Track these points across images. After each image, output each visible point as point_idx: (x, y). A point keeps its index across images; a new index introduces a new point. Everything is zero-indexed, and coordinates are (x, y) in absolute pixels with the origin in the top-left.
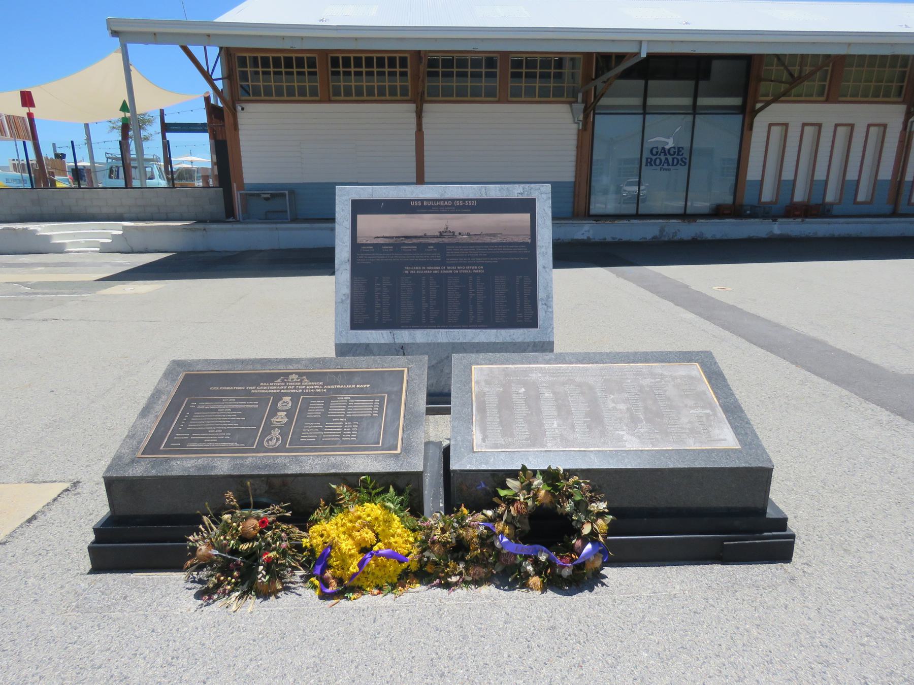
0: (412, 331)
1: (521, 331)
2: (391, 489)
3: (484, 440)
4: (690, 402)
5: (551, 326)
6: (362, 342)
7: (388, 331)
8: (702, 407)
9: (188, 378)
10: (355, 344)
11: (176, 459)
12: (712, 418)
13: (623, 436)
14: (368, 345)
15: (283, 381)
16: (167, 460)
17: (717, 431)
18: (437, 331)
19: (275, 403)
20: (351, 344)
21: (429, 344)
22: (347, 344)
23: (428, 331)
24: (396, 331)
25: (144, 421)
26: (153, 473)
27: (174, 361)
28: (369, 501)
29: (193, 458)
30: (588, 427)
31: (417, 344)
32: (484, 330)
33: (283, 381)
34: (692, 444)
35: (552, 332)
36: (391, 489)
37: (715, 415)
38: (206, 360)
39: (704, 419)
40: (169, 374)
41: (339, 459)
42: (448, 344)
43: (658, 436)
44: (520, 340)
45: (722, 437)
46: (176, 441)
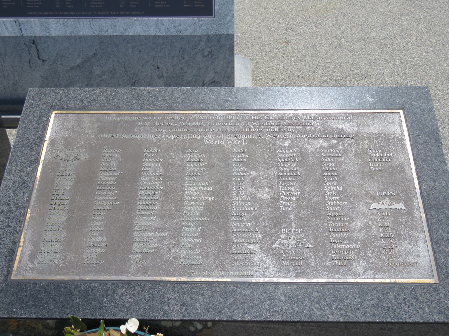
0: (43, 19)
1: (189, 20)
3: (32, 258)
4: (374, 188)
5: (230, 13)
7: (12, 20)
8: (391, 198)
12: (403, 219)
13: (253, 254)
17: (405, 247)
18: (77, 19)
21: (69, 38)
23: (66, 19)
24: (22, 20)
30: (202, 234)
31: (54, 38)
32: (140, 19)
34: (362, 276)
35: (231, 21)
37: (409, 212)
39: (390, 223)
43: (309, 255)
44: (188, 33)
45: (410, 259)
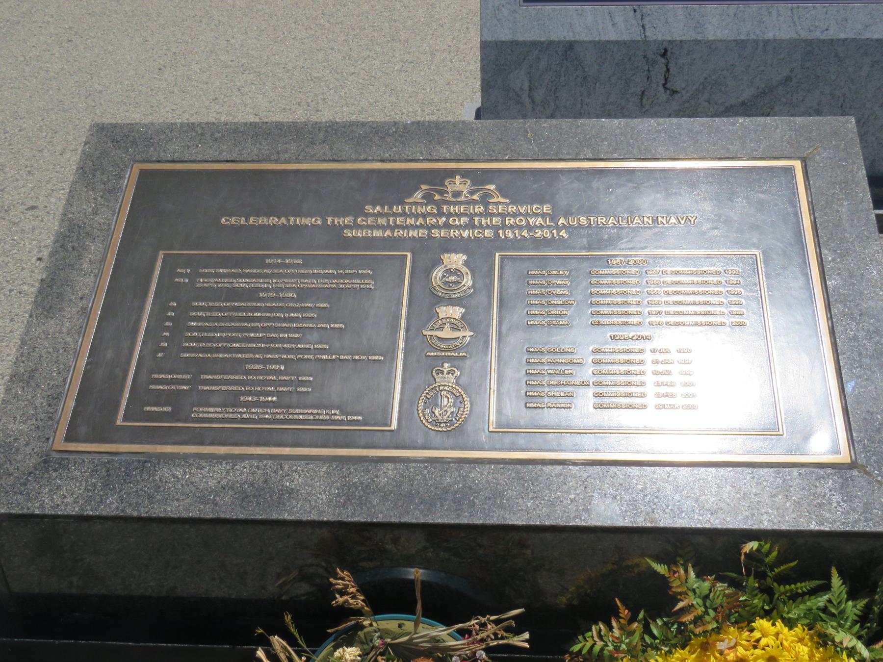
2: (836, 581)
6: (554, 37)
9: (151, 185)
10: (535, 44)
11: (170, 458)
14: (570, 46)
15: (428, 198)
16: (148, 462)
19: (422, 272)
20: (524, 43)
22: (515, 44)
25: (51, 325)
26: (111, 506)
27: (100, 129)
28: (767, 614)
29: (220, 458)
31: (709, 44)
33: (428, 198)
36: (836, 581)
38: (192, 127)
40: (93, 170)
41: (210, 154)
42: (793, 44)
46: (159, 399)
